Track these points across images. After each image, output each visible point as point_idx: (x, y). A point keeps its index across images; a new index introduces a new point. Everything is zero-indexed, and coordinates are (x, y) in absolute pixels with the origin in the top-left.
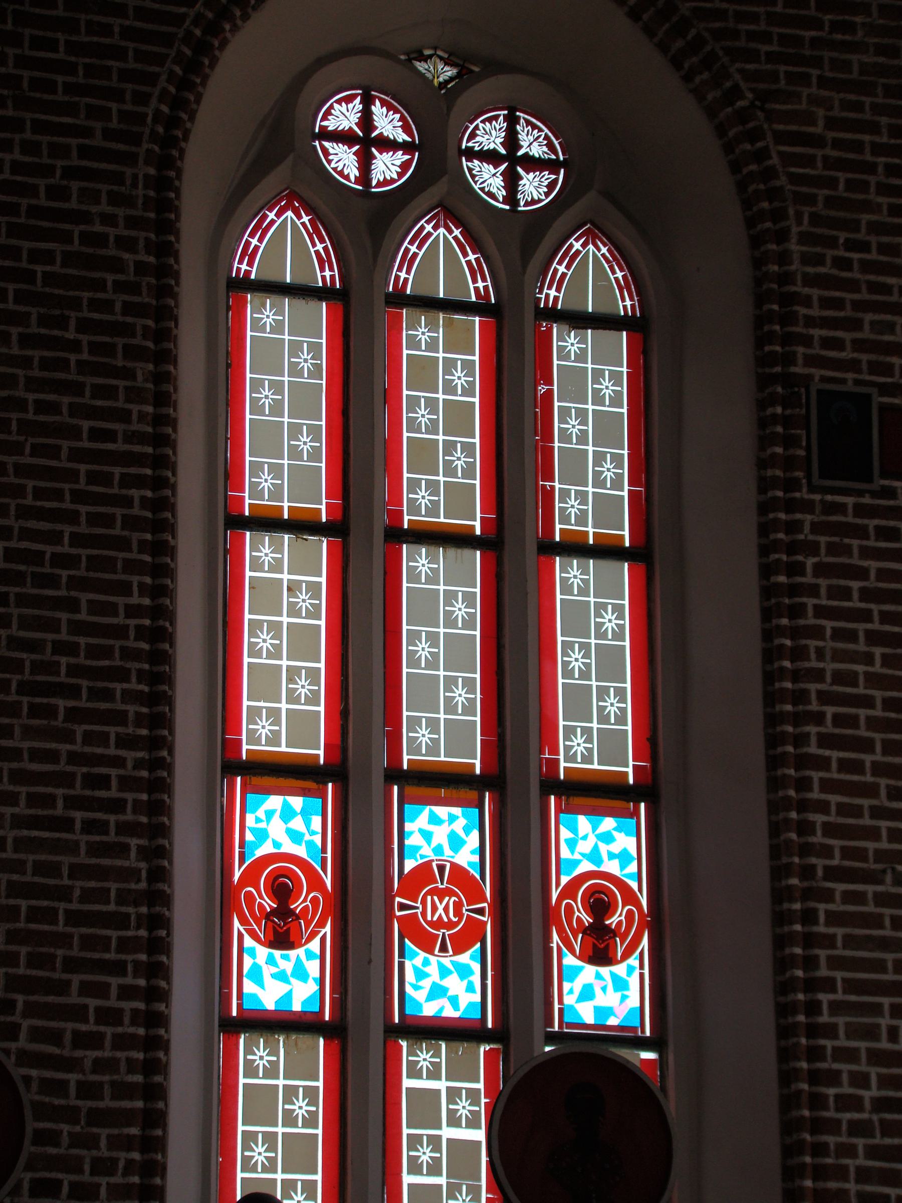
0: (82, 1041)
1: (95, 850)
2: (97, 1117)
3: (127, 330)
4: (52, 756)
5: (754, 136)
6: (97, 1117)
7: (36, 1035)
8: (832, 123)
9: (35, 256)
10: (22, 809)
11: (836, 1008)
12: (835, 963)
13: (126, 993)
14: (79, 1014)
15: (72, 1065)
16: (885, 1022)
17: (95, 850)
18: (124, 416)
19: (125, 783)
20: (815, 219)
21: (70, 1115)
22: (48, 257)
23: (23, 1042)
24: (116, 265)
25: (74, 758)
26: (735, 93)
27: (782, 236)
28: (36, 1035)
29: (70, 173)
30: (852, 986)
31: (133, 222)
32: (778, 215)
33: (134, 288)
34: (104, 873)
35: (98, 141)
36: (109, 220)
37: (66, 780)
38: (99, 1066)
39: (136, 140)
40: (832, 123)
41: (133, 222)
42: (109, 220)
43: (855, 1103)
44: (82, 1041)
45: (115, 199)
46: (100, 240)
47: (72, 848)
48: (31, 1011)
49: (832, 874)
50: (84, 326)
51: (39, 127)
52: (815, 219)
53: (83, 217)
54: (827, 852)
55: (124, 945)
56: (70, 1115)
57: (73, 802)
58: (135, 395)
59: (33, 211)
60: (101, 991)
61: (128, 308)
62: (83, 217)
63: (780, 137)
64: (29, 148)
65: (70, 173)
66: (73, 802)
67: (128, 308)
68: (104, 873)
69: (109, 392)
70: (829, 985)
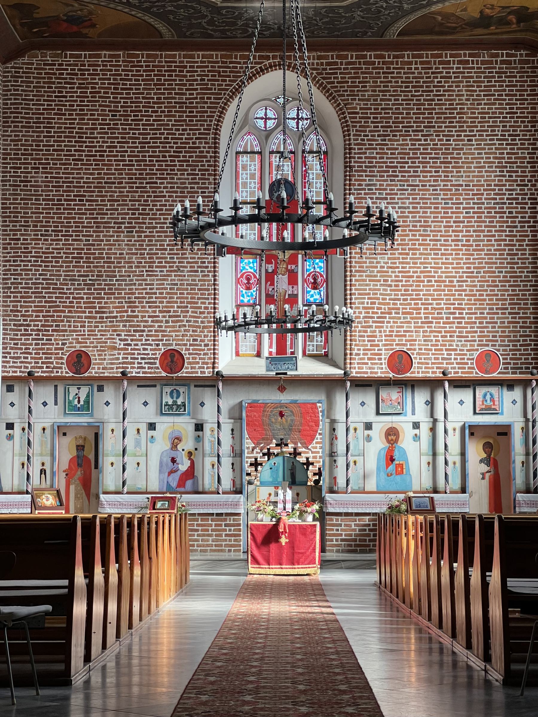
0: (201, 313)
1: (203, 276)
2: (204, 327)
3: (208, 170)
4: (194, 258)
5: (343, 113)
6: (204, 327)
7: (192, 312)
8: (361, 109)
9: (190, 157)
10: (189, 269)
11: (356, 299)
12: (356, 290)
13: (209, 303)
14: (200, 308)
15: (199, 317)
16: (366, 301)
17: (203, 276)
18: (208, 188)
19: (209, 262)
20: (357, 131)
21: (199, 327)
22: (192, 157)
23: (190, 313)
24: (206, 157)
25: (198, 258)
26: (340, 104)
27: (349, 135)
28: (192, 312)
29: (196, 139)
30: (359, 294)
31: (209, 147)
32: (348, 130)
33: (209, 161)
34: (205, 281)
35: (202, 131)
36: (204, 147)
37: (197, 263)
38: (205, 317)
39: (210, 130)
40: (361, 109)
41: (209, 147)
42: (204, 147)
43: (359, 317)
44: (201, 313)
45: (206, 143)
46: (203, 152)
47: (198, 276)
48: (191, 308)
49: (356, 271)
50: (199, 170)
51: (190, 130)
52: (357, 131)
53: (199, 148)
54: (355, 267)
55: (209, 294)
56: (199, 327)
57: (198, 267)
58: (210, 183)
59: (189, 148)
60: (205, 303)
61: (208, 166)
62: (199, 148)
63: (349, 113)
64: (189, 134)
65: (196, 139)
66: (198, 267)
67: (208, 166)
68: (205, 281)
69: (205, 183)
70: (355, 294)
